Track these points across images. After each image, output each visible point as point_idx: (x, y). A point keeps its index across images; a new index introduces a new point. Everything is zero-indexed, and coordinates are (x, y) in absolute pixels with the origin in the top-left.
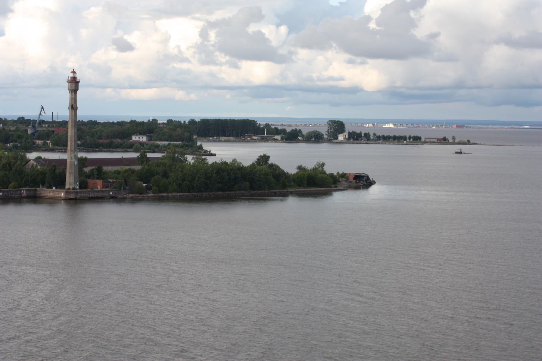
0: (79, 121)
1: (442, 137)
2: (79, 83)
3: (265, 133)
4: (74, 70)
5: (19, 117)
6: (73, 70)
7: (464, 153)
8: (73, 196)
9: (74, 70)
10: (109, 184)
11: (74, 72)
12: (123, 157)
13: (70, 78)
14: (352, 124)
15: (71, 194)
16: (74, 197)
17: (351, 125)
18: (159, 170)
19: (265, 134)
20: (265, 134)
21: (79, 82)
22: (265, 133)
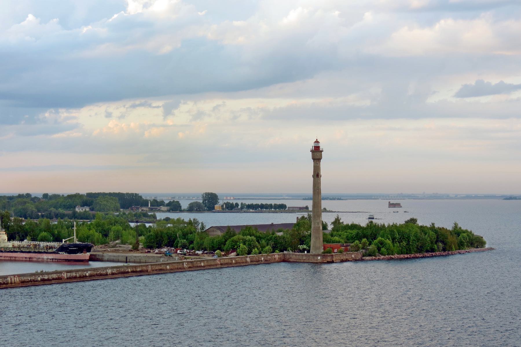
0: (33, 197)
1: (305, 206)
2: (322, 152)
3: (149, 205)
4: (317, 140)
5: (43, 194)
6: (316, 140)
7: (376, 219)
8: (330, 259)
9: (317, 140)
10: (344, 247)
11: (317, 142)
12: (433, 224)
13: (313, 147)
14: (151, 197)
15: (328, 258)
16: (331, 260)
17: (180, 198)
18: (180, 233)
19: (149, 206)
20: (149, 206)
21: (323, 151)
22: (149, 205)
